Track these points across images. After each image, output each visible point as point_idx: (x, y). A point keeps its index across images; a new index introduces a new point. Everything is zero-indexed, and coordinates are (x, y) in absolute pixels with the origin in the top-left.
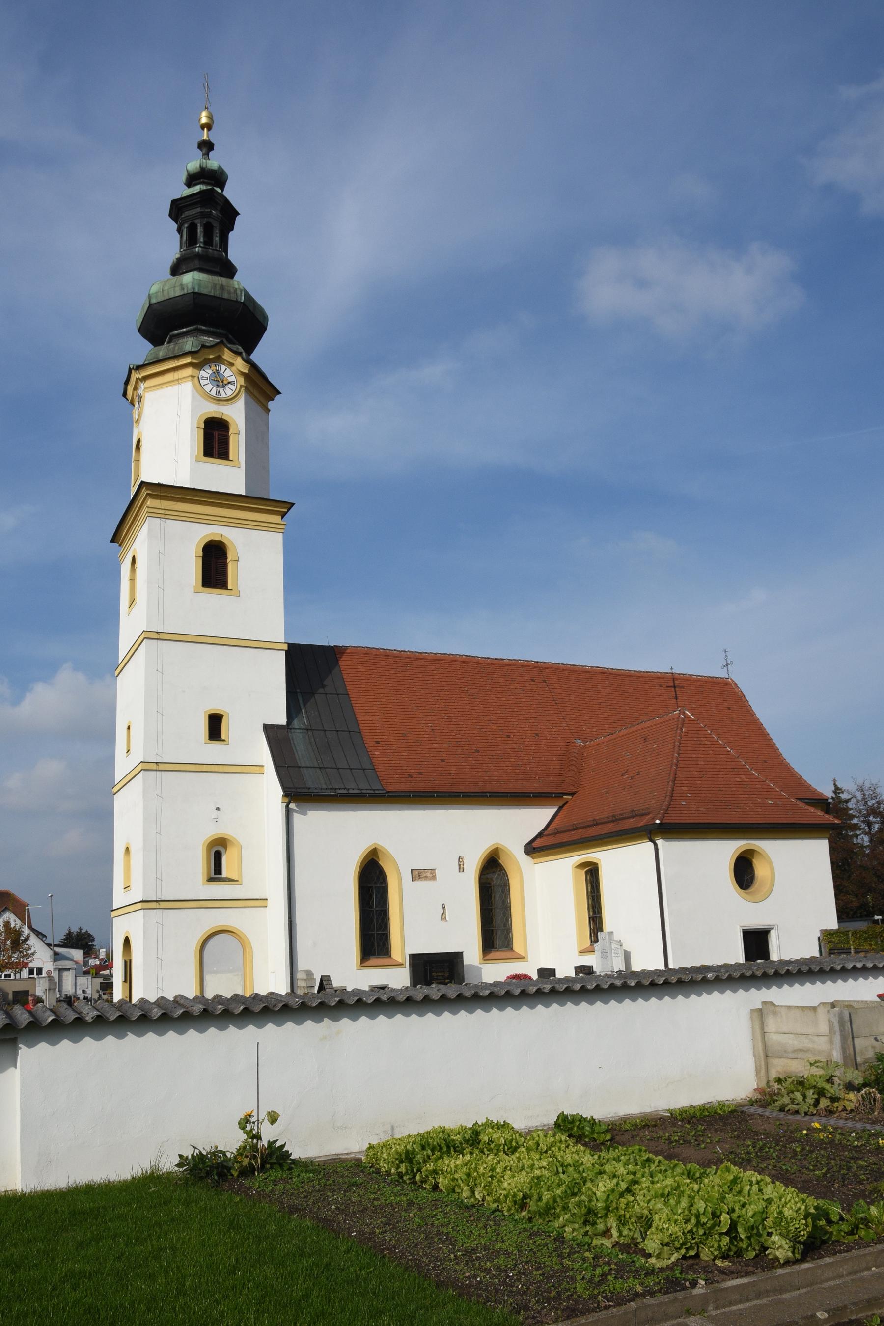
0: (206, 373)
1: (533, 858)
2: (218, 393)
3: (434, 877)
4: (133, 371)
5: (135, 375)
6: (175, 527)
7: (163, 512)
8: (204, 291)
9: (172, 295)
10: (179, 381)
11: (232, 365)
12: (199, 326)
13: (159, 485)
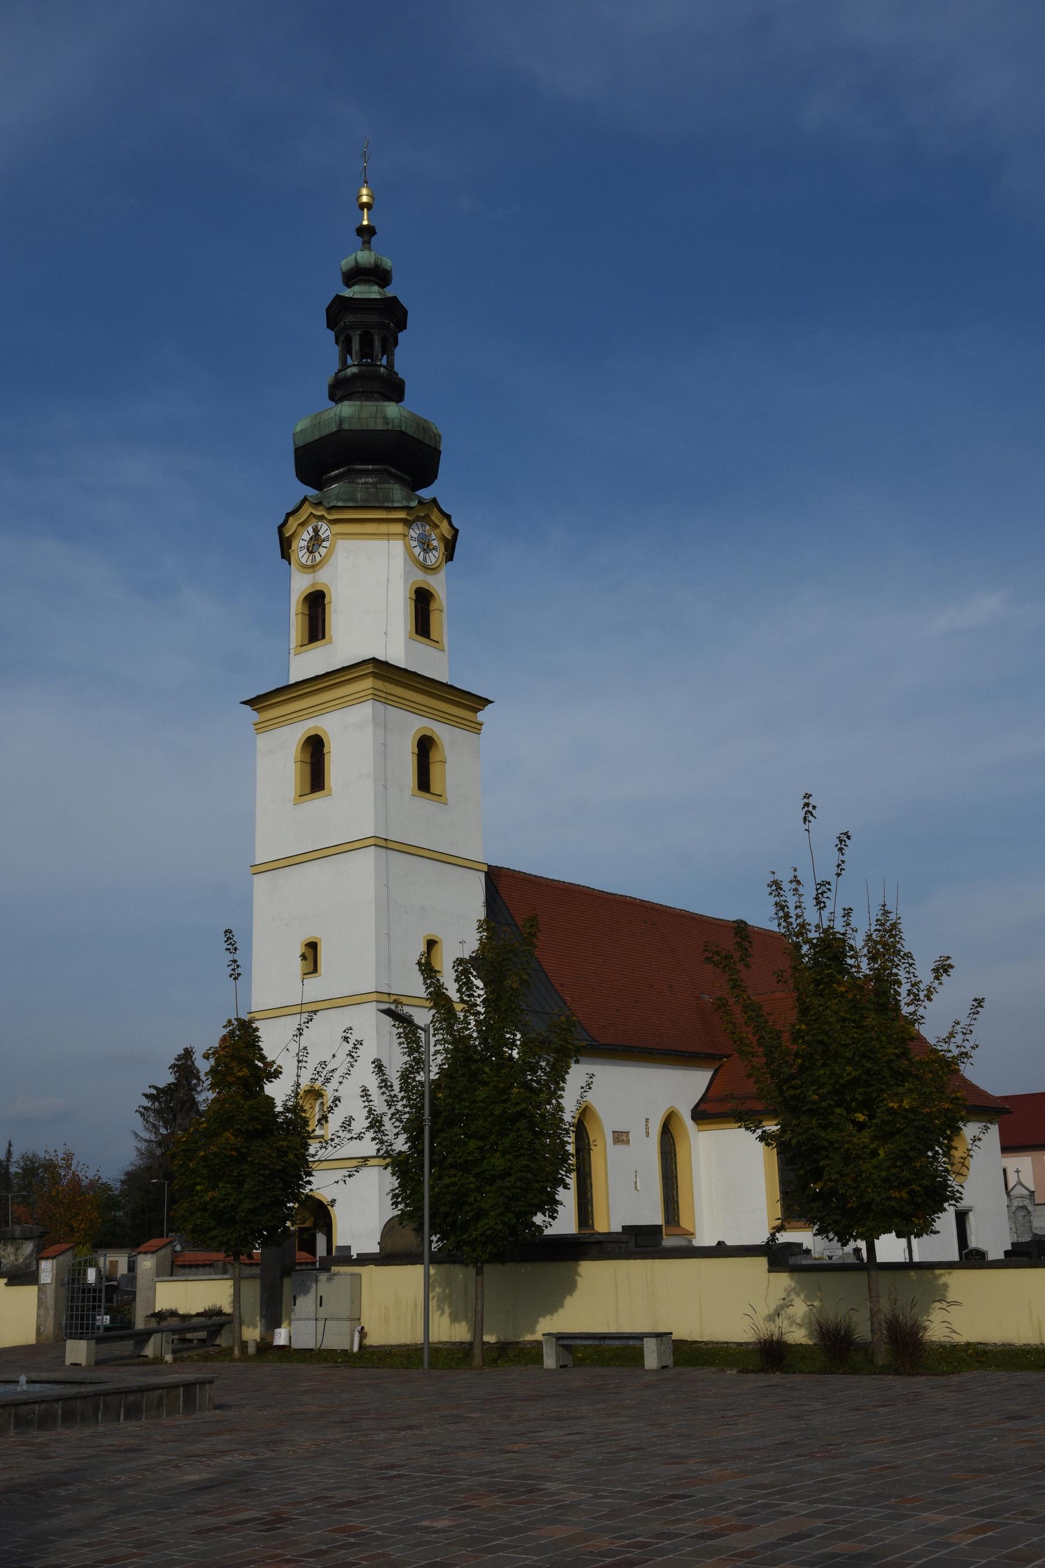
0: (414, 533)
1: (698, 1124)
2: (425, 559)
3: (628, 1142)
4: (307, 504)
5: (307, 510)
6: (395, 714)
7: (383, 695)
8: (410, 431)
9: (372, 427)
10: (388, 536)
11: (437, 527)
12: (390, 468)
13: (386, 664)
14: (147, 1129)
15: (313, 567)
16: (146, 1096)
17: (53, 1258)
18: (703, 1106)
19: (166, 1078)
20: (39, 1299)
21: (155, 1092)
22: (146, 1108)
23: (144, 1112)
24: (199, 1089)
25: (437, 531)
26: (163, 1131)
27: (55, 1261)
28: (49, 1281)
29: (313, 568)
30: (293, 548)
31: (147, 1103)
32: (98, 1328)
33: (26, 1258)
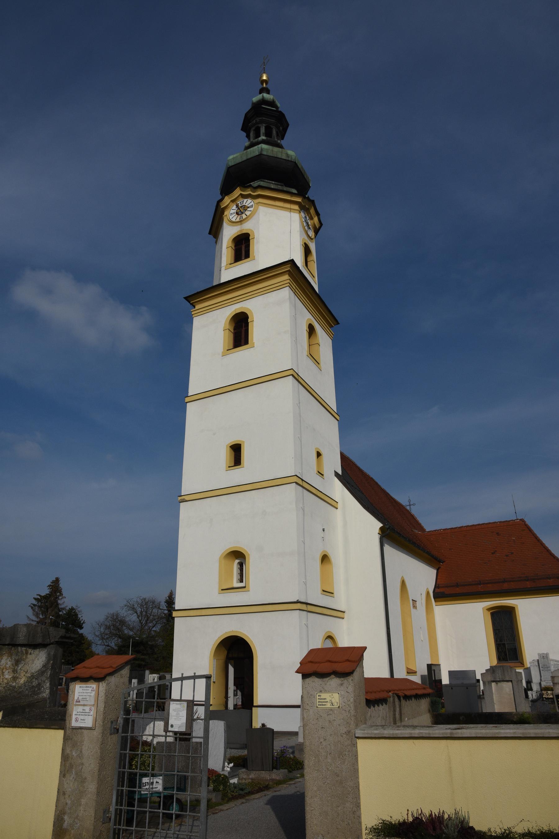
10: (291, 210)
14: (34, 615)
15: (241, 221)
16: (35, 599)
17: (98, 679)
18: (438, 590)
19: (45, 591)
20: (65, 757)
21: (39, 597)
22: (34, 605)
23: (33, 607)
24: (60, 598)
25: (312, 221)
26: (41, 616)
27: (103, 686)
28: (88, 722)
29: (241, 222)
30: (225, 214)
31: (35, 602)
32: (143, 800)
33: (33, 676)
